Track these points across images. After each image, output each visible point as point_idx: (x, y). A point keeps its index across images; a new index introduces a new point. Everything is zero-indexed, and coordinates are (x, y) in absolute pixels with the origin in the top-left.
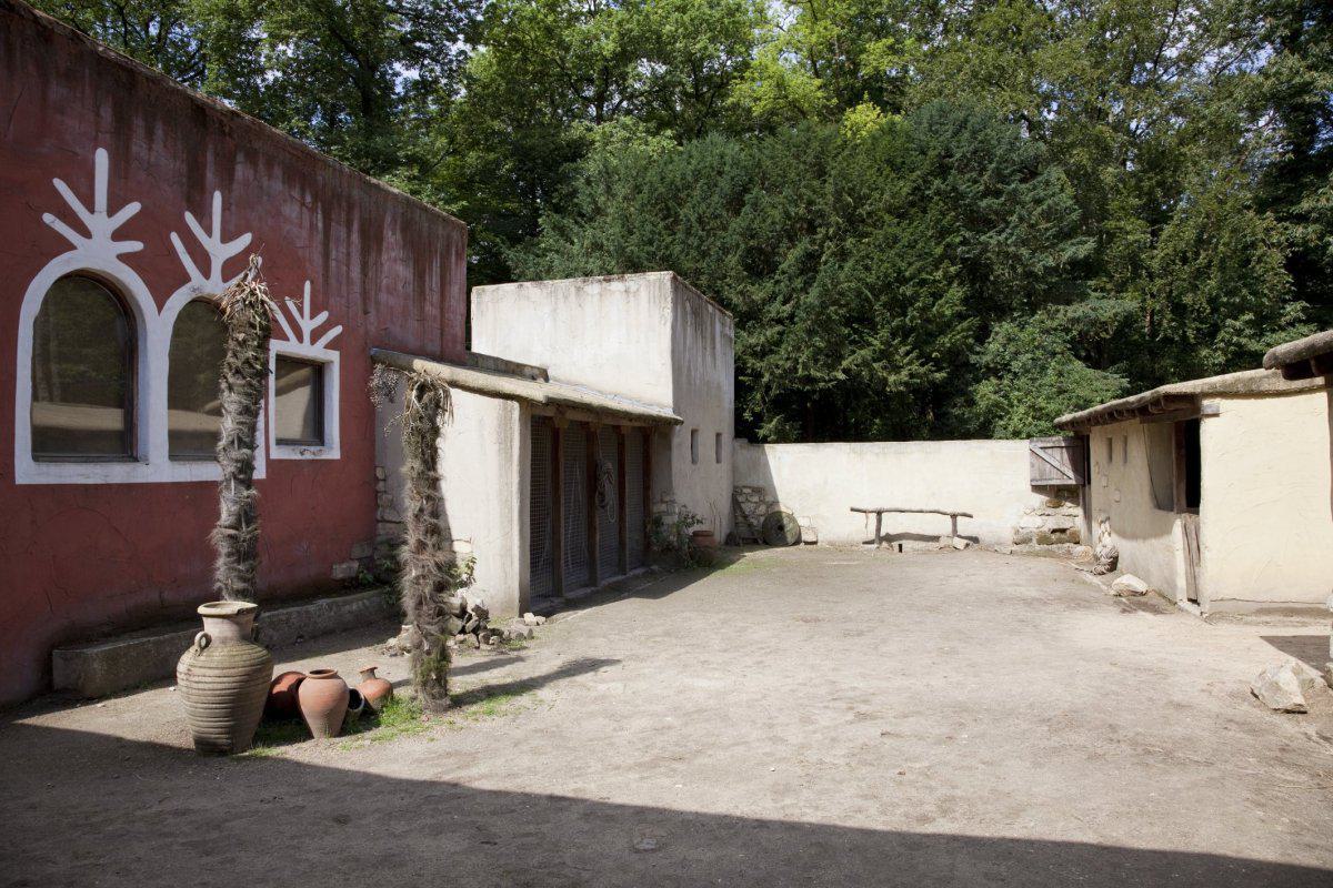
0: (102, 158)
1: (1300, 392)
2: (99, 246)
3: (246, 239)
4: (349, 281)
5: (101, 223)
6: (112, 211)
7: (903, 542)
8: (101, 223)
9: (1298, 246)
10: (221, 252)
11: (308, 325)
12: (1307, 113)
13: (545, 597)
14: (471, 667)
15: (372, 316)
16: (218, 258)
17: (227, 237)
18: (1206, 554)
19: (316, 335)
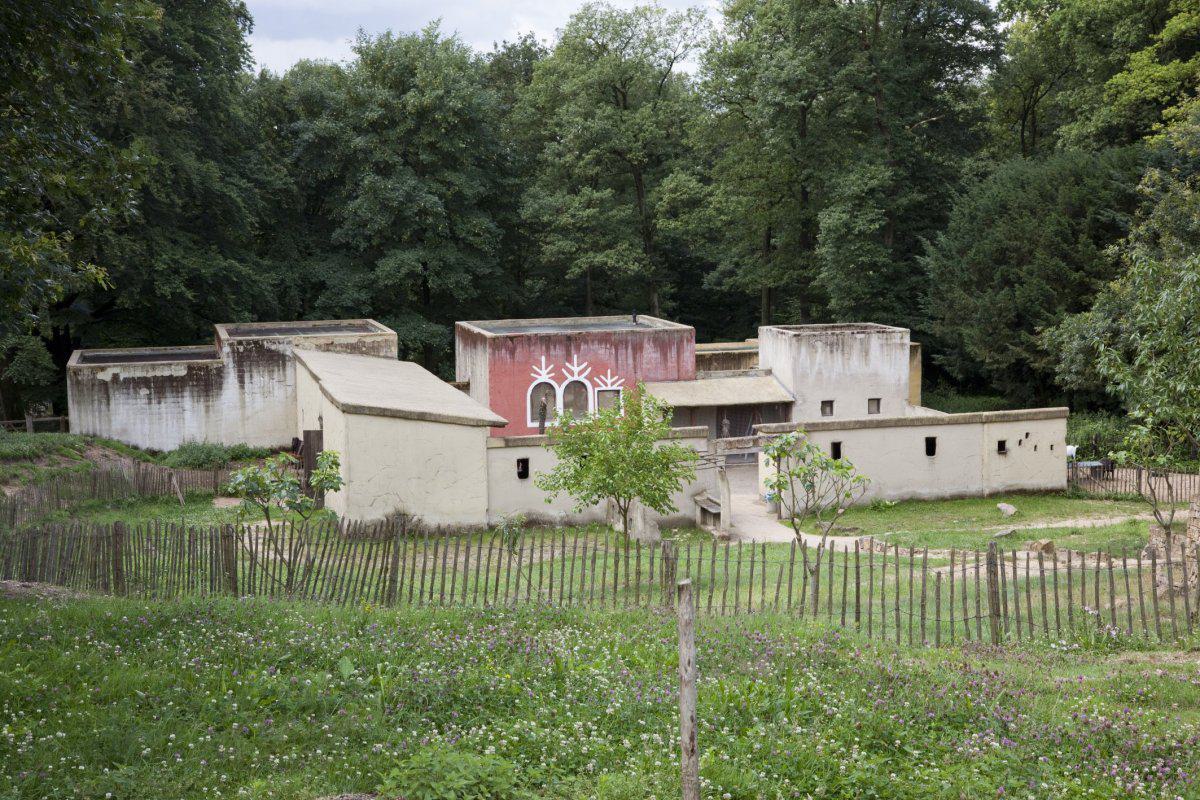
0: (543, 359)
1: (967, 422)
2: (544, 376)
3: (585, 364)
4: (628, 365)
5: (544, 372)
6: (547, 368)
7: (845, 438)
8: (544, 372)
9: (726, 214)
10: (576, 369)
11: (609, 381)
12: (440, 109)
13: (930, 386)
14: (912, 420)
15: (639, 373)
16: (577, 370)
17: (579, 365)
18: (329, 403)
19: (613, 384)
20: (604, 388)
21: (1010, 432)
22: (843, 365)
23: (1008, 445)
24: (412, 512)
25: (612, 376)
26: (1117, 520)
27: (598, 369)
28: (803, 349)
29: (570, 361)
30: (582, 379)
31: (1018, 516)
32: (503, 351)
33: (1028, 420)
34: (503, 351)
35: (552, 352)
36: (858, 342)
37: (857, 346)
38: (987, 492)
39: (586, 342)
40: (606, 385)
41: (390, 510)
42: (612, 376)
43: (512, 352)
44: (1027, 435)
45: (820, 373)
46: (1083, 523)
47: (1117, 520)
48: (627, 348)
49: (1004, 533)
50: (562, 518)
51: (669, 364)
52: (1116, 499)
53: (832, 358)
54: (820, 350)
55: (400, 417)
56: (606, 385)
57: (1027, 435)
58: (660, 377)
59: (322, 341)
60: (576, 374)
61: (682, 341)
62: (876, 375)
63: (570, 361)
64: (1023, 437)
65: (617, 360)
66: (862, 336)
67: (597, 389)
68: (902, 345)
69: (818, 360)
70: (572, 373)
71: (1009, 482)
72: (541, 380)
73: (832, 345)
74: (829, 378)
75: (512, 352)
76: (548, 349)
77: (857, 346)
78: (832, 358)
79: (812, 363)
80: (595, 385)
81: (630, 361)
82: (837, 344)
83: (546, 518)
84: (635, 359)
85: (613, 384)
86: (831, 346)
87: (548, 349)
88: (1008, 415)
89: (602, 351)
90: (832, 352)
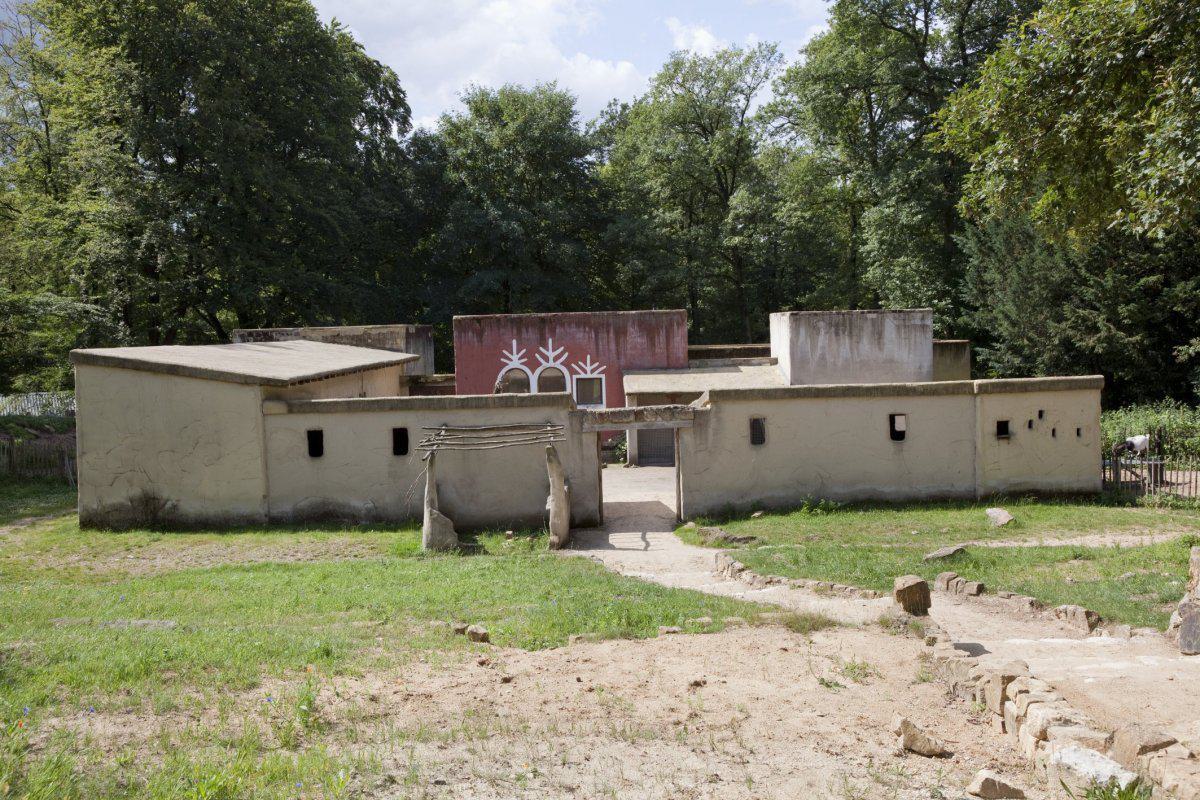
0: (514, 342)
5: (515, 357)
8: (515, 357)
10: (551, 354)
11: (589, 368)
17: (554, 350)
19: (592, 371)
20: (583, 376)
21: (1016, 408)
22: (851, 349)
23: (1012, 427)
24: (165, 495)
25: (592, 363)
26: (1160, 539)
27: (575, 356)
28: (802, 331)
29: (546, 347)
30: (558, 364)
31: (1015, 525)
32: (470, 334)
33: (1040, 390)
34: (470, 334)
35: (524, 335)
36: (869, 323)
37: (868, 328)
38: (981, 492)
39: (562, 325)
40: (585, 372)
41: (136, 492)
42: (592, 363)
43: (480, 334)
44: (1041, 414)
45: (823, 357)
46: (1127, 540)
47: (1160, 539)
48: (608, 332)
49: (947, 553)
50: (369, 511)
51: (658, 350)
52: (1175, 507)
53: (838, 340)
54: (822, 332)
55: (145, 370)
56: (585, 372)
57: (1041, 414)
58: (647, 365)
59: (328, 334)
60: (551, 359)
61: (672, 325)
62: (891, 361)
63: (546, 347)
64: (1035, 417)
65: (597, 344)
66: (874, 316)
67: (575, 377)
68: (924, 327)
69: (820, 344)
70: (546, 359)
71: (1015, 480)
72: (511, 365)
73: (837, 325)
74: (835, 364)
75: (480, 334)
76: (519, 332)
77: (868, 328)
78: (838, 340)
79: (814, 346)
80: (572, 372)
81: (613, 346)
82: (844, 325)
83: (347, 510)
84: (617, 344)
85: (592, 371)
86: (837, 328)
87: (519, 332)
88: (1013, 384)
89: (580, 335)
90: (837, 334)
